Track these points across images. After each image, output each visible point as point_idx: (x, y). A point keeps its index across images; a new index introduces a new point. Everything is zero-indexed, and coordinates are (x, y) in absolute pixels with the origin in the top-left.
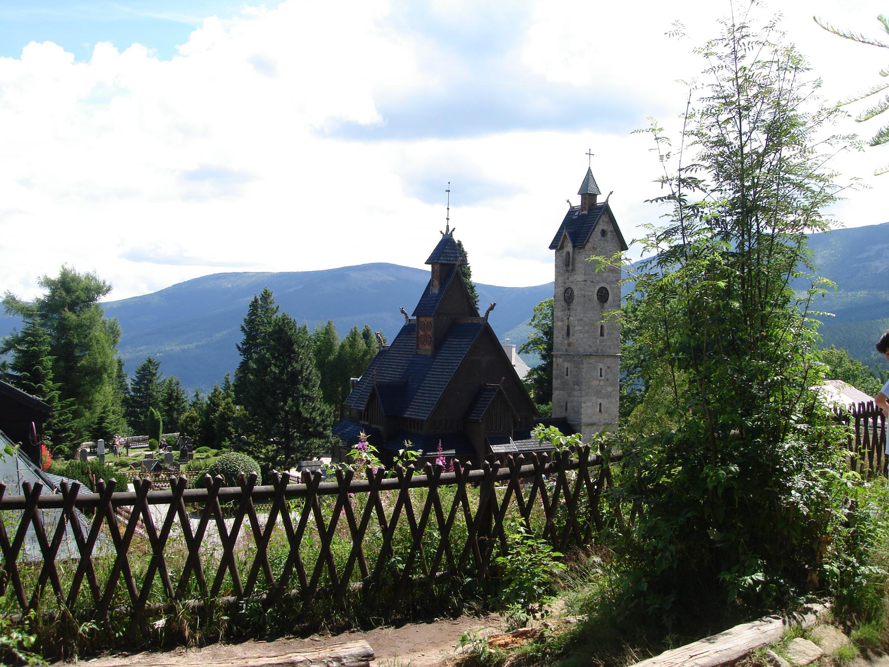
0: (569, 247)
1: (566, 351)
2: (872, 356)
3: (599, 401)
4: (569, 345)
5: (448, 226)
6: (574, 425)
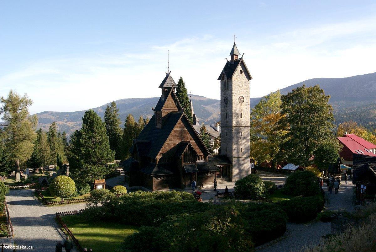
0: (226, 79)
1: (226, 125)
2: (370, 124)
4: (227, 122)
6: (230, 158)
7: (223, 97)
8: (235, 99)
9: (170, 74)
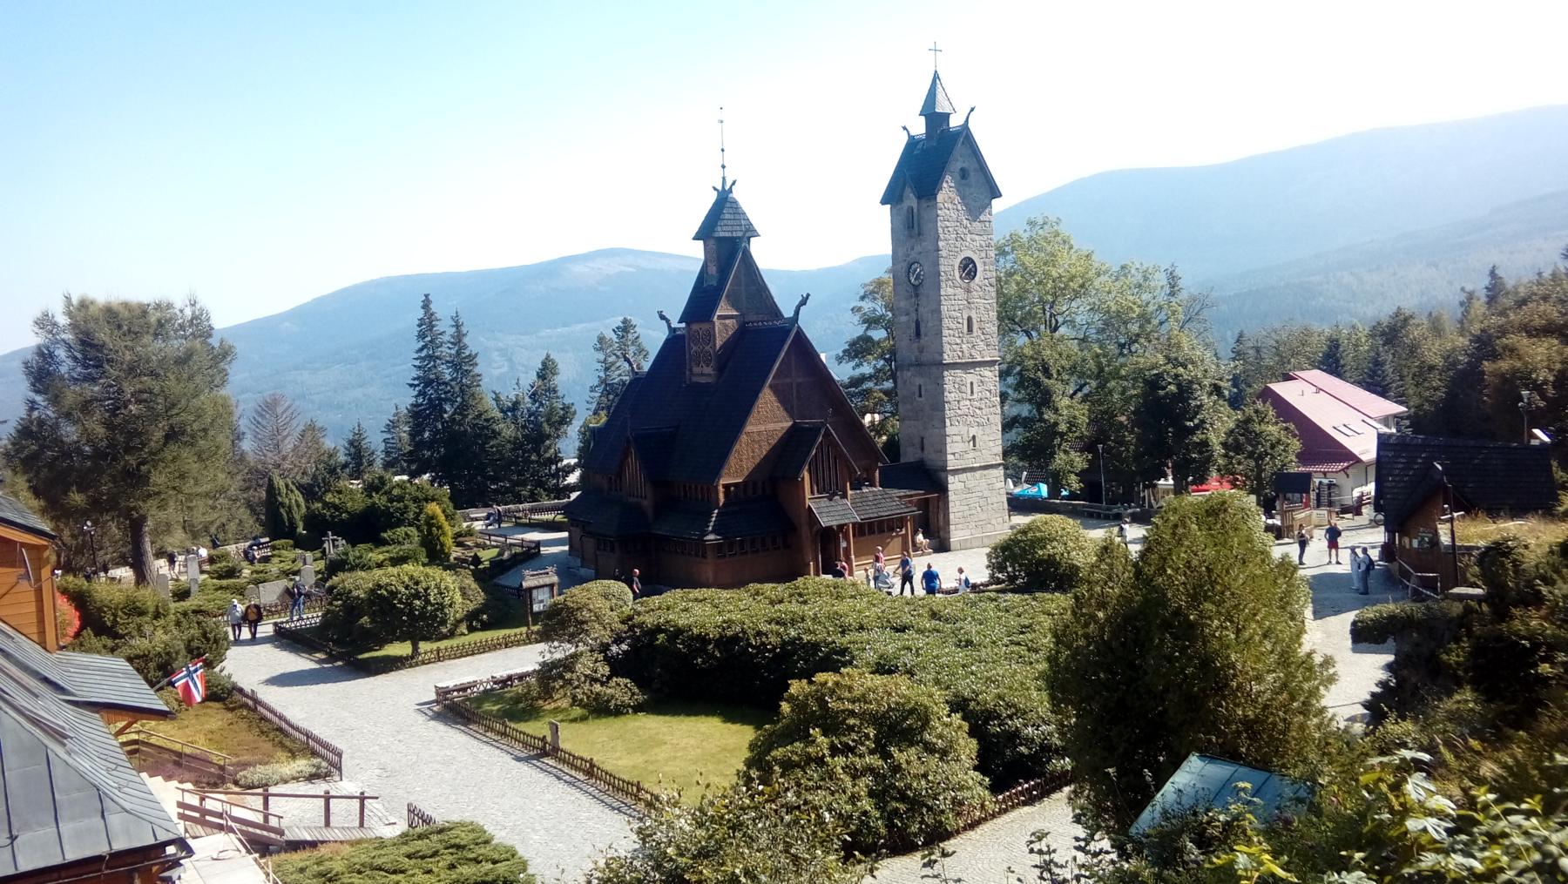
3: (973, 431)
7: (905, 265)
9: (730, 190)
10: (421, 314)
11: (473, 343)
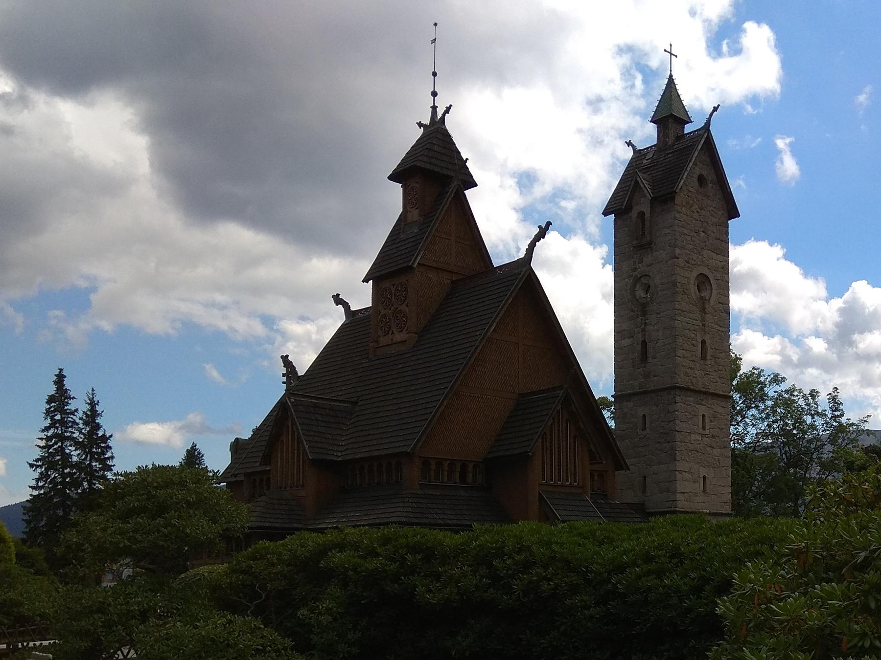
3: (703, 472)
5: (434, 108)
8: (685, 281)
10: (52, 390)
11: (106, 424)
